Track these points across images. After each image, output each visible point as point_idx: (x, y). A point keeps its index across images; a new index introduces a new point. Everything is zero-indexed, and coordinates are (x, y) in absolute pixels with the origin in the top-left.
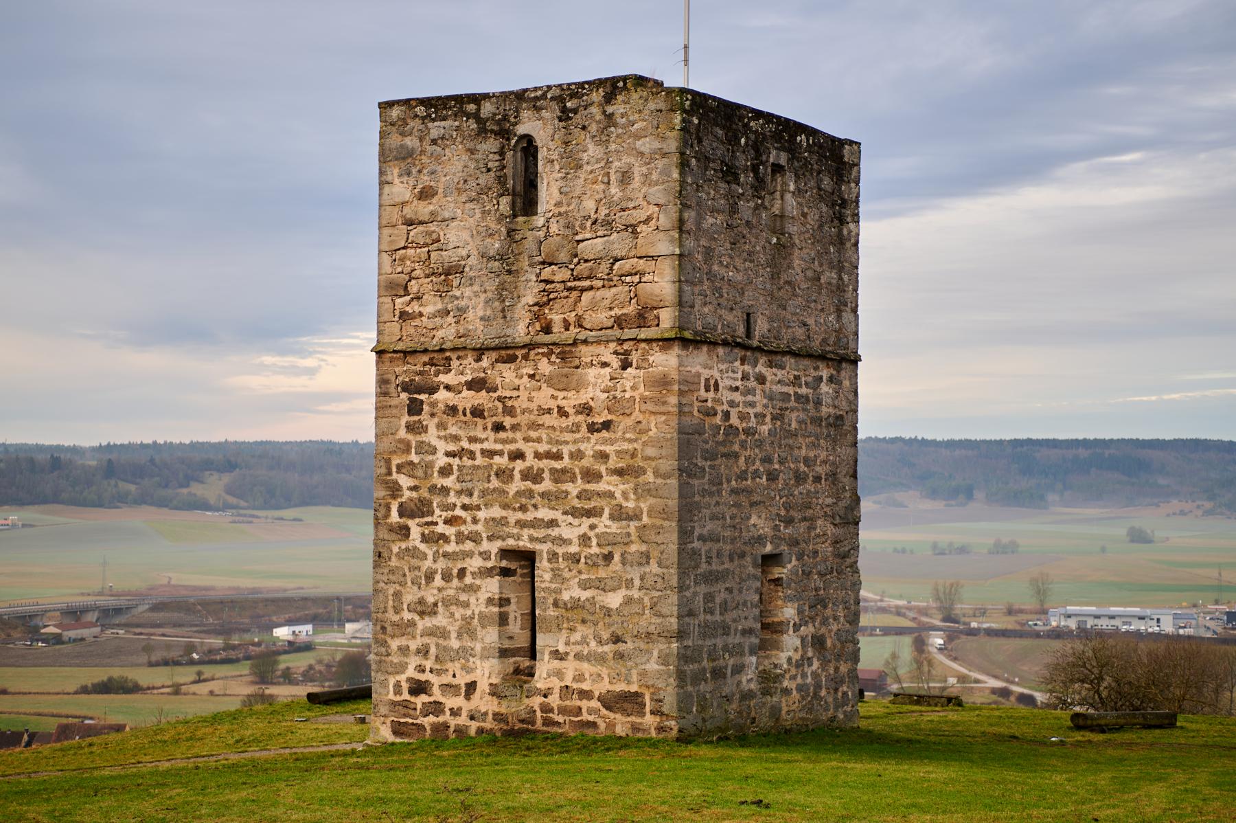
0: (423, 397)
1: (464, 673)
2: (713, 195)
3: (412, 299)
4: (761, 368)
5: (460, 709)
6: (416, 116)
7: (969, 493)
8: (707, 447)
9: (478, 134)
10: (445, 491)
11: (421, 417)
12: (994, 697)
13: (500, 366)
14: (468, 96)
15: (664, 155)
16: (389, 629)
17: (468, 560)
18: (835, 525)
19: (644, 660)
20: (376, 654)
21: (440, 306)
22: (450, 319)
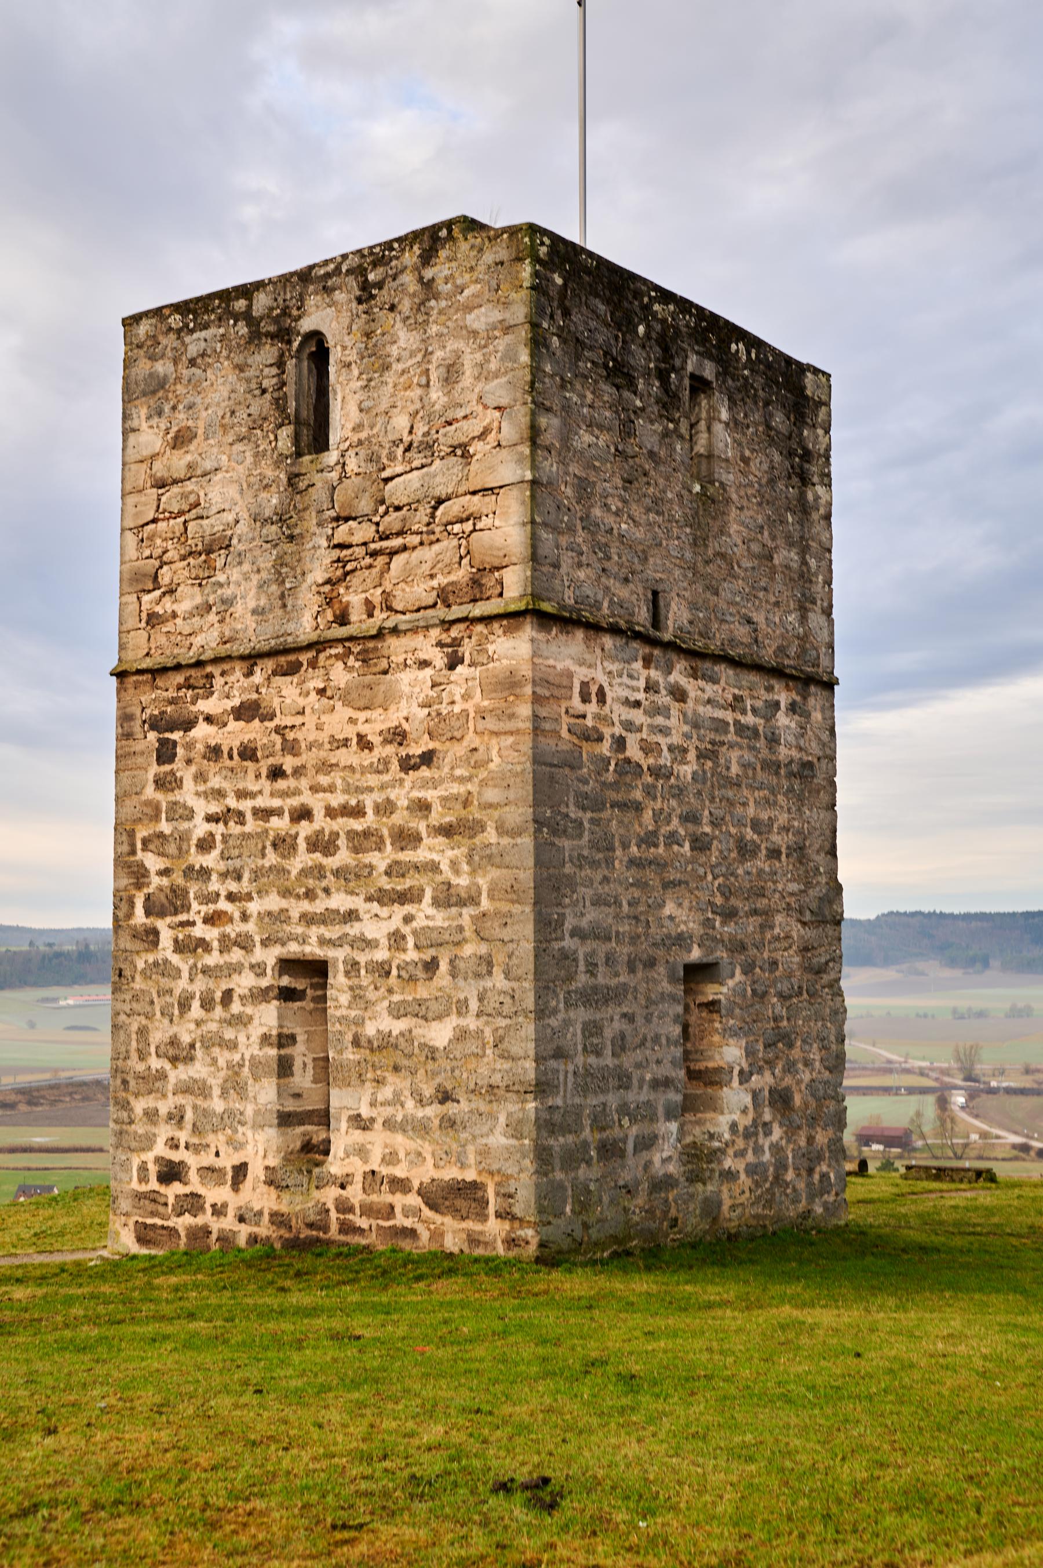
0: (176, 736)
1: (231, 1150)
2: (593, 398)
3: (164, 594)
4: (678, 677)
5: (225, 1205)
6: (170, 329)
7: (986, 964)
8: (587, 788)
9: (249, 342)
10: (205, 873)
11: (174, 766)
12: (1015, 1153)
13: (278, 680)
14: (236, 289)
15: (507, 329)
16: (132, 1083)
17: (235, 977)
18: (804, 924)
19: (485, 1129)
20: (116, 1121)
21: (198, 600)
22: (212, 617)
